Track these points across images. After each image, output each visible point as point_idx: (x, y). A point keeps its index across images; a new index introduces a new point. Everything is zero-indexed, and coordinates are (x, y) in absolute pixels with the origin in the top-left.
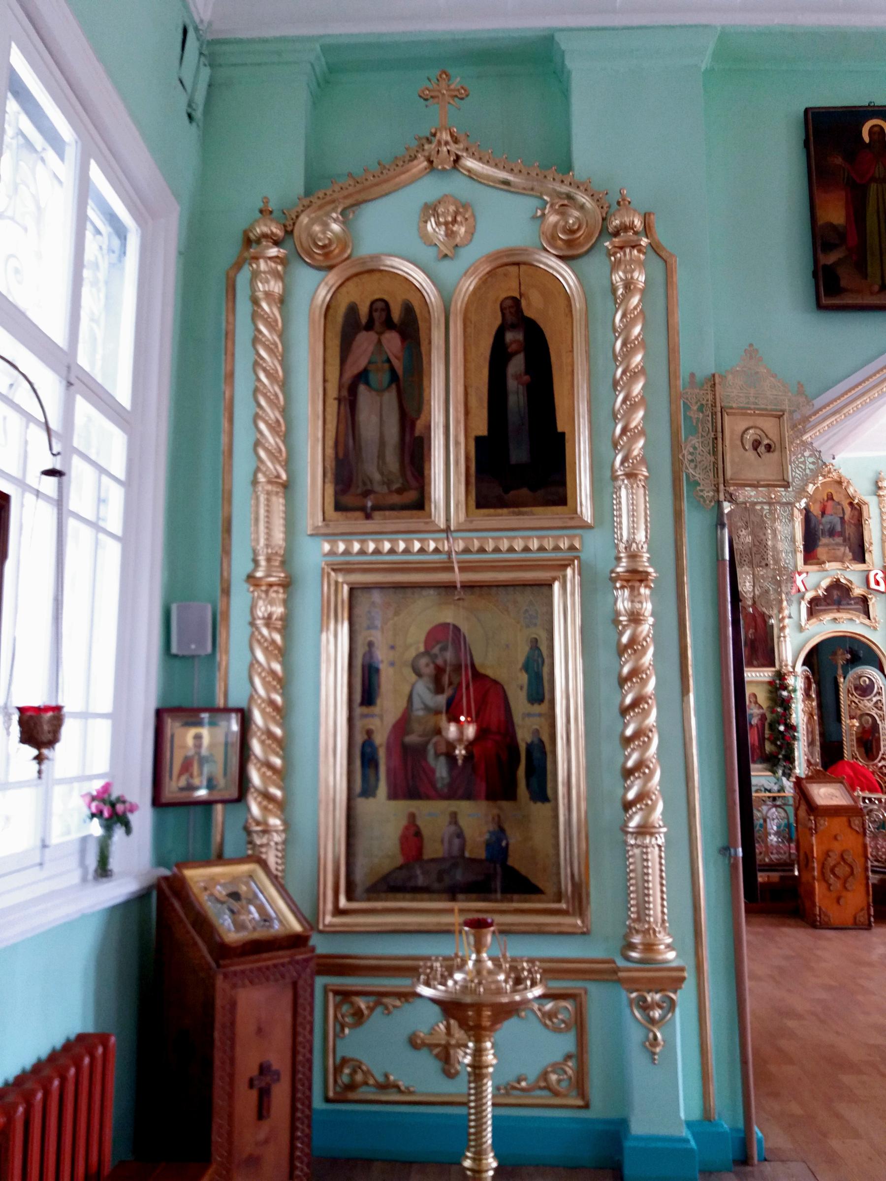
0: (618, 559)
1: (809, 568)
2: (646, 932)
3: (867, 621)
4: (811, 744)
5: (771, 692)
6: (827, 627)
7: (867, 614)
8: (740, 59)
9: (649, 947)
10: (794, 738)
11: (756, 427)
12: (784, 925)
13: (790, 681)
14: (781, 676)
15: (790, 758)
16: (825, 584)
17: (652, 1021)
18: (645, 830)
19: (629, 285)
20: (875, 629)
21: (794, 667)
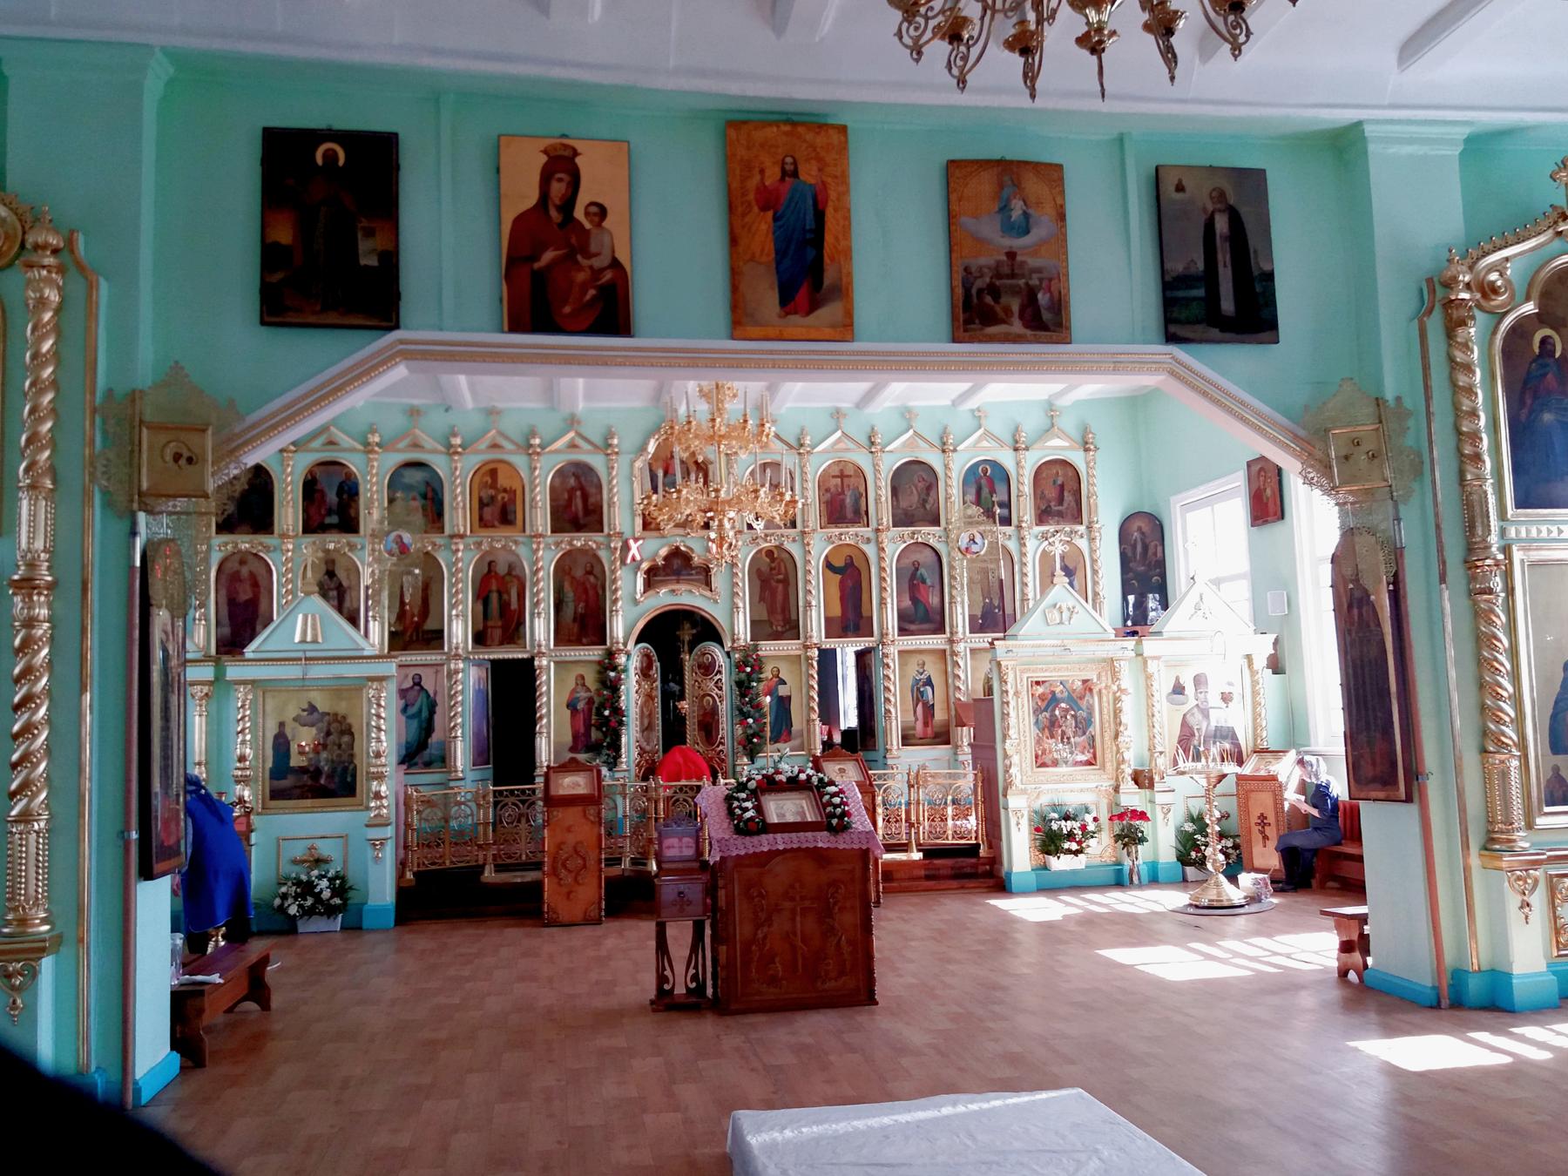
0: (18, 567)
1: (647, 533)
2: (15, 909)
3: (708, 594)
4: (647, 729)
5: (599, 672)
6: (665, 598)
7: (708, 583)
8: (201, 73)
9: (23, 922)
10: (621, 723)
11: (165, 446)
12: (507, 926)
13: (622, 659)
14: (611, 654)
15: (616, 747)
16: (664, 552)
17: (13, 988)
18: (26, 817)
19: (42, 303)
20: (716, 602)
21: (625, 644)
